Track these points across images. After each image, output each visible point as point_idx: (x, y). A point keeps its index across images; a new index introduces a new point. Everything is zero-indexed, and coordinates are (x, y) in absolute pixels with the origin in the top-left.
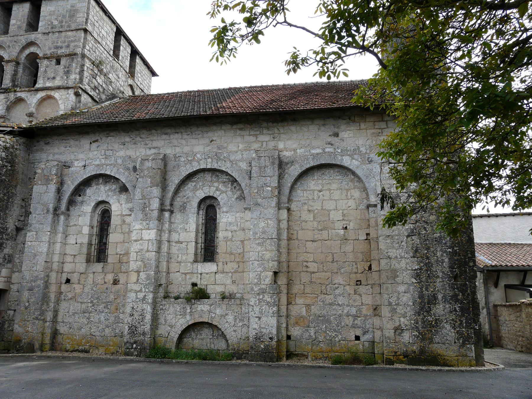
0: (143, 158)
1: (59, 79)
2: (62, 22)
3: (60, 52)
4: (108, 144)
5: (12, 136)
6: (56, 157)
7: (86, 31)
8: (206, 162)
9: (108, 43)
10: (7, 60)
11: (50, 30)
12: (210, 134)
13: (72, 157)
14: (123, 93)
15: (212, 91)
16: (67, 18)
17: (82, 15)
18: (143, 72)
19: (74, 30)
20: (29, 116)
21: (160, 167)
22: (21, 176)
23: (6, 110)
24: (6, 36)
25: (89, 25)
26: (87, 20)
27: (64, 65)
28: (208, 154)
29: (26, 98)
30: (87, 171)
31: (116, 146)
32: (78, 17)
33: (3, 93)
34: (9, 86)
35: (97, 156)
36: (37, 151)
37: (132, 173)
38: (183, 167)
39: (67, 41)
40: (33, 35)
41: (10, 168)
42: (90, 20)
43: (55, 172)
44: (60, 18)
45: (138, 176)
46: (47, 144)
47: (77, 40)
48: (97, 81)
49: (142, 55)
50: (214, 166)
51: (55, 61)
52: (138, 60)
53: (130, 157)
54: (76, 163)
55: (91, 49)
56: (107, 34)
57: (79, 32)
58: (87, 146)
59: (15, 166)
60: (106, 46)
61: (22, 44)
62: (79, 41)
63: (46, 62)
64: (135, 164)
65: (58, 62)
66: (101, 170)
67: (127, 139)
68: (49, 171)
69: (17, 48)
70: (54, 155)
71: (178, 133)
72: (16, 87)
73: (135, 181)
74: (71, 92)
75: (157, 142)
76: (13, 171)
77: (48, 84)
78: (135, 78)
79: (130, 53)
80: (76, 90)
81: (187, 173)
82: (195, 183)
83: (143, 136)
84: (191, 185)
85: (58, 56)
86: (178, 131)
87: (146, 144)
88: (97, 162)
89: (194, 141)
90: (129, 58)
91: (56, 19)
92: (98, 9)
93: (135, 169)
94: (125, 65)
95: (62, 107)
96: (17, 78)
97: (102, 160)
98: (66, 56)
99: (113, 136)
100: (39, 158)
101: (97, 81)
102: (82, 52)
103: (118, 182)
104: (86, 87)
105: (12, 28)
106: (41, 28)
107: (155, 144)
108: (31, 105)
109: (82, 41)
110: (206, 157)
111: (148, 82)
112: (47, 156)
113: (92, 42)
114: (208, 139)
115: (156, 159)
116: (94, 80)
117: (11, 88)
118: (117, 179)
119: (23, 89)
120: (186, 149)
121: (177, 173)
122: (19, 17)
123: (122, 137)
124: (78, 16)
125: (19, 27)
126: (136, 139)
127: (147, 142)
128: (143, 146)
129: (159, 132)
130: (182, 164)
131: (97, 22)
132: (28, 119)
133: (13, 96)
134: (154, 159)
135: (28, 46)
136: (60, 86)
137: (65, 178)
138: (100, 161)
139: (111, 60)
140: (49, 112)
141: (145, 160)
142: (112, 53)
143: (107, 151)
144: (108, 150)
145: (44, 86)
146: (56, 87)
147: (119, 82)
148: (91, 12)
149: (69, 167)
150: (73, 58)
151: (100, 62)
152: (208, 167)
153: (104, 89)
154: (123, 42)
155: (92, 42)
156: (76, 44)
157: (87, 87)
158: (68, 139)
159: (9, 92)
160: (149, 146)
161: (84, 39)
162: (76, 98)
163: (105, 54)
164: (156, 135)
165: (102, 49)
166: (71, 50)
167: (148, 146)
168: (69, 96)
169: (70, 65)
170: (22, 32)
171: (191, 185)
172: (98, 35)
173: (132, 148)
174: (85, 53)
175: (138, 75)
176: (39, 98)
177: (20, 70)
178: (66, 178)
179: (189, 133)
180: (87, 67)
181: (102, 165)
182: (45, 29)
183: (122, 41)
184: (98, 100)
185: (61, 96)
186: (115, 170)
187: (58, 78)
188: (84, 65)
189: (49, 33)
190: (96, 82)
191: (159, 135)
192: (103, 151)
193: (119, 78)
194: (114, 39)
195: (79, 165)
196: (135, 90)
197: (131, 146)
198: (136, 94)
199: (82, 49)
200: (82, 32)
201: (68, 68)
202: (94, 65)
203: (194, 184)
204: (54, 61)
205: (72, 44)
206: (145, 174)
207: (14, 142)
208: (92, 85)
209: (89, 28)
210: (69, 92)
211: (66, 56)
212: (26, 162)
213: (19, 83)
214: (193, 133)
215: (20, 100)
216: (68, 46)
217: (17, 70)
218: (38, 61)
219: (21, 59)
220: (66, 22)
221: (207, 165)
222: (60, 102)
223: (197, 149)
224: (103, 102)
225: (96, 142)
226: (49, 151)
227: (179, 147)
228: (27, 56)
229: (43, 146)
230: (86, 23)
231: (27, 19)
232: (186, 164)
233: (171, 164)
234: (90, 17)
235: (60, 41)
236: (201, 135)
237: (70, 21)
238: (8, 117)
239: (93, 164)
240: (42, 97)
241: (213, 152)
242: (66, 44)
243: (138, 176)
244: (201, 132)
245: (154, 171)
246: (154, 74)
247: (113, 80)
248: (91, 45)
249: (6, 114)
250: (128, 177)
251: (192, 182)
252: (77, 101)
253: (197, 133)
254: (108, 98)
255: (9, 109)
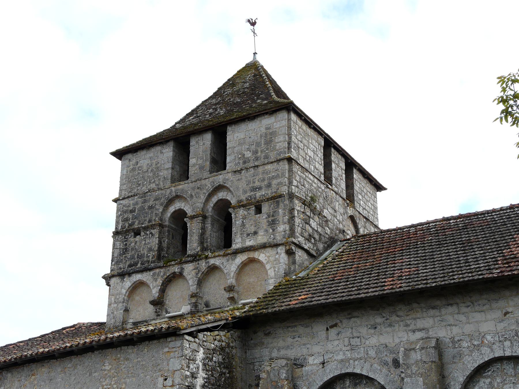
0: (406, 346)
1: (262, 234)
2: (256, 152)
3: (258, 194)
4: (352, 329)
5: (226, 331)
6: (283, 352)
7: (290, 160)
8: (502, 346)
9: (317, 165)
10: (191, 216)
11: (241, 166)
12: (502, 303)
13: (305, 351)
14: (344, 231)
15: (483, 213)
16: (263, 146)
17: (281, 138)
18: (365, 191)
19: (275, 161)
20: (229, 291)
21: (434, 360)
22: (240, 383)
23: (197, 285)
24: (186, 182)
25: (292, 150)
26: (289, 143)
27: (267, 213)
28: (503, 333)
29: (221, 266)
30: (328, 371)
31: (364, 331)
32: (278, 143)
33: (191, 262)
34: (197, 250)
35: (338, 348)
36: (256, 345)
37: (393, 369)
38: (467, 357)
39: (266, 179)
40: (221, 176)
41: (228, 375)
42: (293, 142)
43: (284, 375)
44: (253, 147)
45: (403, 375)
46: (268, 334)
47: (280, 176)
48: (311, 227)
49: (361, 166)
50: (516, 352)
51: (254, 208)
52: (356, 175)
53: (386, 346)
54: (311, 360)
55: (299, 184)
56: (314, 153)
57: (281, 163)
58: (323, 334)
59: (233, 372)
60: (315, 170)
61: (207, 190)
62: (283, 175)
63: (242, 212)
64: (394, 355)
65: (259, 210)
66: (347, 368)
67: (379, 320)
68: (277, 374)
69: (202, 197)
70: (279, 350)
71: (451, 305)
72: (205, 250)
73: (399, 382)
74: (281, 250)
75: (423, 321)
76: (231, 378)
77: (249, 243)
78: (356, 203)
79: (344, 168)
80: (288, 248)
81: (476, 365)
82: (489, 380)
83: (400, 313)
84: (484, 383)
85: (258, 202)
86: (451, 302)
87: (407, 325)
88: (341, 357)
89: (478, 316)
90: (344, 176)
91: (248, 149)
92: (300, 123)
93: (396, 363)
94: (340, 189)
95: (271, 273)
96: (205, 238)
97: (347, 352)
98: (268, 200)
99: (358, 317)
100: (258, 356)
101: (311, 227)
102: (289, 191)
103: (373, 383)
104: (299, 239)
105: (192, 170)
106: (230, 164)
107: (420, 324)
108: (229, 274)
109: (287, 175)
110: (501, 339)
111: (373, 203)
112: (270, 352)
113: (299, 172)
114: (500, 312)
115: (427, 348)
116: (307, 227)
117: (200, 253)
118: (371, 380)
119: (217, 254)
120: (468, 329)
121: (460, 365)
122: (200, 154)
123: (371, 318)
124: (276, 141)
125: (202, 168)
126: (391, 318)
127: (408, 322)
128: (402, 328)
129: (423, 305)
130: (466, 351)
131: (301, 142)
132: (227, 295)
133: (204, 264)
134: (423, 348)
135: (216, 191)
136: (265, 244)
137: (298, 383)
138: (344, 354)
139: (323, 188)
140: (254, 282)
141: (410, 350)
142: (322, 178)
143: (351, 340)
144: (353, 338)
145: (244, 246)
146: (260, 246)
147: (336, 217)
148: (293, 132)
149: (302, 366)
150: (278, 203)
151: (312, 198)
152: (506, 355)
153: (320, 235)
154: (335, 156)
155: (299, 172)
156: (279, 180)
157: (301, 239)
158: (296, 326)
159: (198, 260)
160: (412, 327)
161: (289, 171)
162: (288, 258)
163: (315, 183)
164: (420, 310)
165: (312, 177)
166: (274, 190)
167: (410, 328)
168: (279, 257)
169: (275, 211)
170: (206, 174)
171: (484, 383)
172: (305, 159)
173: (388, 333)
174: (293, 191)
175: (358, 197)
176: (238, 264)
177: (209, 226)
178: (299, 383)
179: (469, 303)
180: (298, 211)
181: (348, 360)
182: (236, 165)
183: (333, 155)
184: (315, 254)
185: (269, 257)
186: (367, 366)
187: (261, 233)
188: (293, 209)
189: (242, 170)
190: (310, 229)
191: (424, 310)
192: (346, 340)
193: (335, 211)
194: (322, 158)
195: (315, 362)
196: (358, 222)
197: (384, 330)
198: (361, 231)
199: (289, 187)
200: (286, 162)
201: (273, 216)
202: (305, 205)
203: (488, 381)
204: (253, 209)
205: (274, 182)
206: (414, 371)
207: (229, 338)
208: (306, 234)
209: (294, 154)
210: (279, 251)
211: (268, 200)
212: (243, 362)
213: (209, 244)
214: (476, 304)
215: (213, 269)
216: (269, 186)
217: (204, 226)
218: (230, 210)
219: (208, 210)
220: (262, 152)
221: (504, 351)
222: (268, 267)
223: (485, 327)
224: (321, 254)
225: (335, 328)
226: (272, 345)
227: (456, 326)
228: (214, 205)
229: (262, 339)
230: (289, 148)
231: (210, 154)
232: (471, 351)
233: (449, 352)
234: (293, 138)
235: (257, 180)
236: (487, 306)
237: (267, 149)
238: (201, 295)
239: (335, 360)
240: (242, 262)
241: (512, 331)
242: (266, 182)
243: (403, 375)
244: (486, 301)
245: (426, 366)
246: (379, 188)
247: (329, 217)
248: (298, 178)
249: (198, 290)
250: (387, 376)
251: (486, 377)
252: (291, 261)
253: (480, 302)
254: (326, 246)
255: (201, 282)
